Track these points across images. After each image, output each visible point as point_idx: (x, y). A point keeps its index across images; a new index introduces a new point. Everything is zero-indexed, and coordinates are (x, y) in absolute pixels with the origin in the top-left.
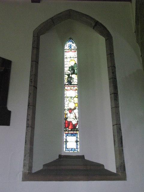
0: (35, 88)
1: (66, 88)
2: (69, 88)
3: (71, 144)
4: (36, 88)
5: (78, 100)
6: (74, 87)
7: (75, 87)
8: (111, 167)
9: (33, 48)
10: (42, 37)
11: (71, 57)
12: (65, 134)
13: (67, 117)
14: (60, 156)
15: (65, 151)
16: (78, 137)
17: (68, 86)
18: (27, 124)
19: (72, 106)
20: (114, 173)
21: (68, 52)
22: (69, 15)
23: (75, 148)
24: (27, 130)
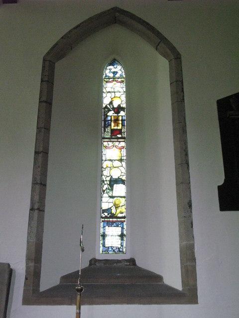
0: (43, 185)
1: (105, 144)
2: (111, 144)
3: (113, 237)
4: (45, 185)
5: (127, 190)
6: (120, 142)
7: (121, 143)
8: (173, 279)
9: (34, 183)
10: (58, 65)
11: (114, 93)
12: (102, 224)
13: (108, 179)
14: (93, 261)
15: (100, 254)
16: (125, 227)
17: (111, 141)
18: (34, 179)
19: (116, 174)
20: (177, 290)
21: (110, 82)
22: (115, 17)
23: (119, 246)
24: (33, 191)
